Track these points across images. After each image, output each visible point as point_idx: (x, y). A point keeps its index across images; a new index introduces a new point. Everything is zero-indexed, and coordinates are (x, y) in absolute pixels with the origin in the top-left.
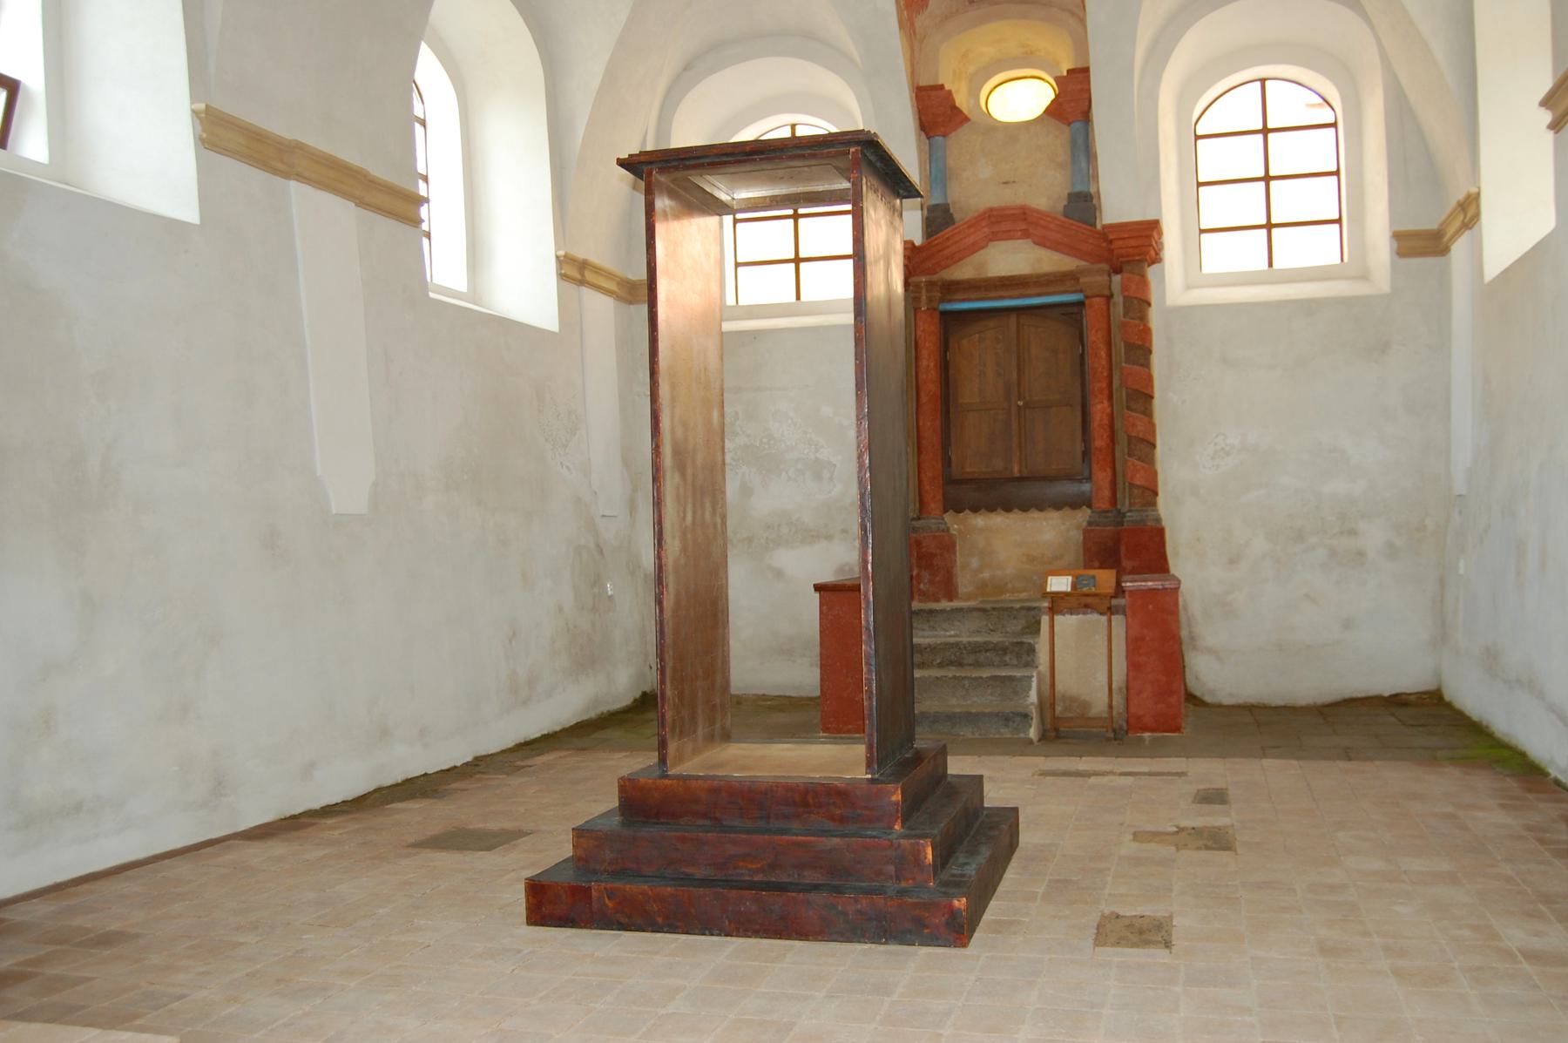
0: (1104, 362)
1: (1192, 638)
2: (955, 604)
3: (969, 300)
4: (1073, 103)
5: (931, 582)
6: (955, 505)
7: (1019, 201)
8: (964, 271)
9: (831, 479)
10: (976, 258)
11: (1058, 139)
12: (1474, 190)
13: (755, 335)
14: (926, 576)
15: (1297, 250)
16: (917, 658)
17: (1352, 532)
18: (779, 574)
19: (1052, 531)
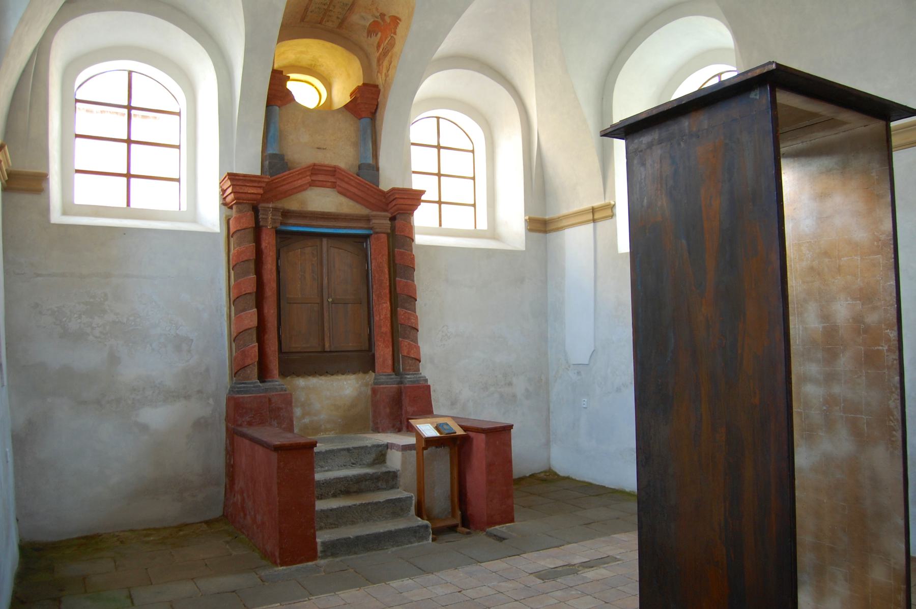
0: (387, 276)
3: (340, 228)
4: (367, 105)
6: (286, 372)
9: (189, 351)
10: (300, 196)
12: (613, 203)
13: (124, 231)
15: (146, 196)
16: (317, 492)
17: (510, 384)
18: (144, 428)
19: (346, 388)
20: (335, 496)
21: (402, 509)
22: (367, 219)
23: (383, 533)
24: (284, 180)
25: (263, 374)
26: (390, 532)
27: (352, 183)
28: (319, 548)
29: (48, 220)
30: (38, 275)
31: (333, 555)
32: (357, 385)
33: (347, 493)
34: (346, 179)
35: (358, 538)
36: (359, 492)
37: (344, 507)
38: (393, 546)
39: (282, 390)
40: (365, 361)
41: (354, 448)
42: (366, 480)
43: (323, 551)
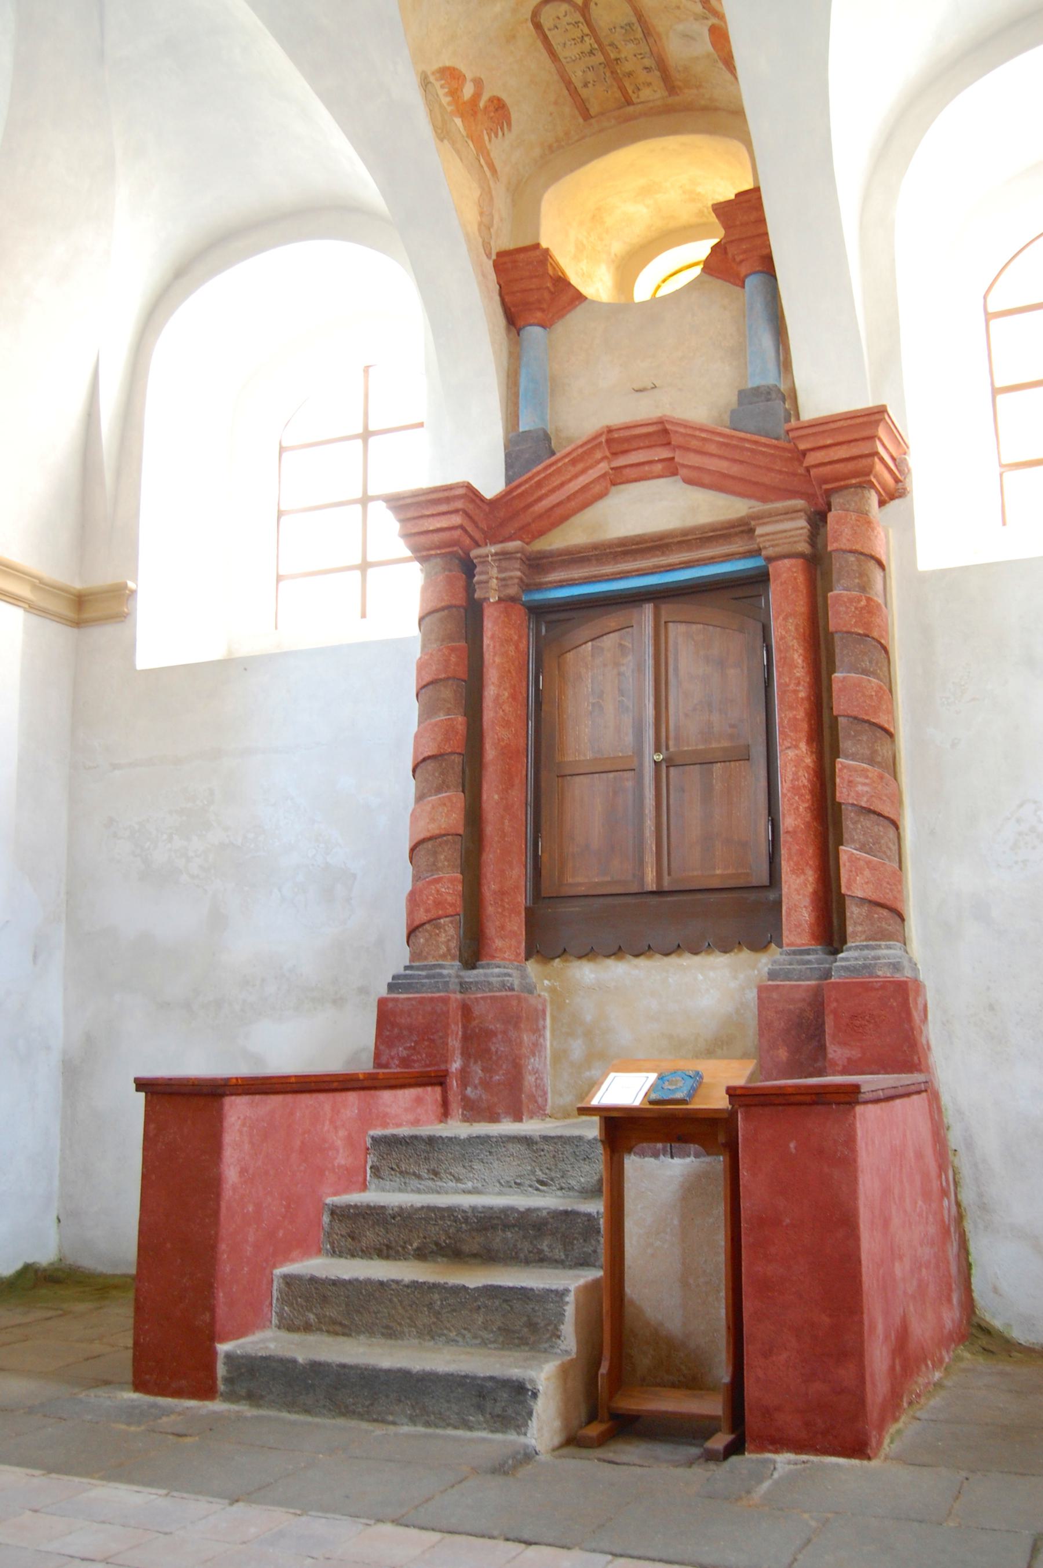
1: (984, 1207)
2: (530, 1127)
5: (486, 1085)
6: (544, 940)
7: (655, 414)
8: (573, 534)
11: (725, 310)
14: (477, 1071)
20: (421, 1255)
21: (532, 1326)
22: (743, 528)
23: (388, 1372)
24: (539, 485)
25: (474, 950)
26: (405, 1375)
27: (712, 448)
28: (221, 1370)
29: (134, 665)
30: (115, 767)
31: (252, 1398)
32: (733, 985)
33: (453, 1253)
34: (694, 444)
35: (316, 1368)
36: (488, 1257)
37: (368, 1282)
38: (413, 1420)
39: (503, 986)
40: (739, 914)
41: (546, 1139)
42: (506, 1227)
43: (228, 1381)
